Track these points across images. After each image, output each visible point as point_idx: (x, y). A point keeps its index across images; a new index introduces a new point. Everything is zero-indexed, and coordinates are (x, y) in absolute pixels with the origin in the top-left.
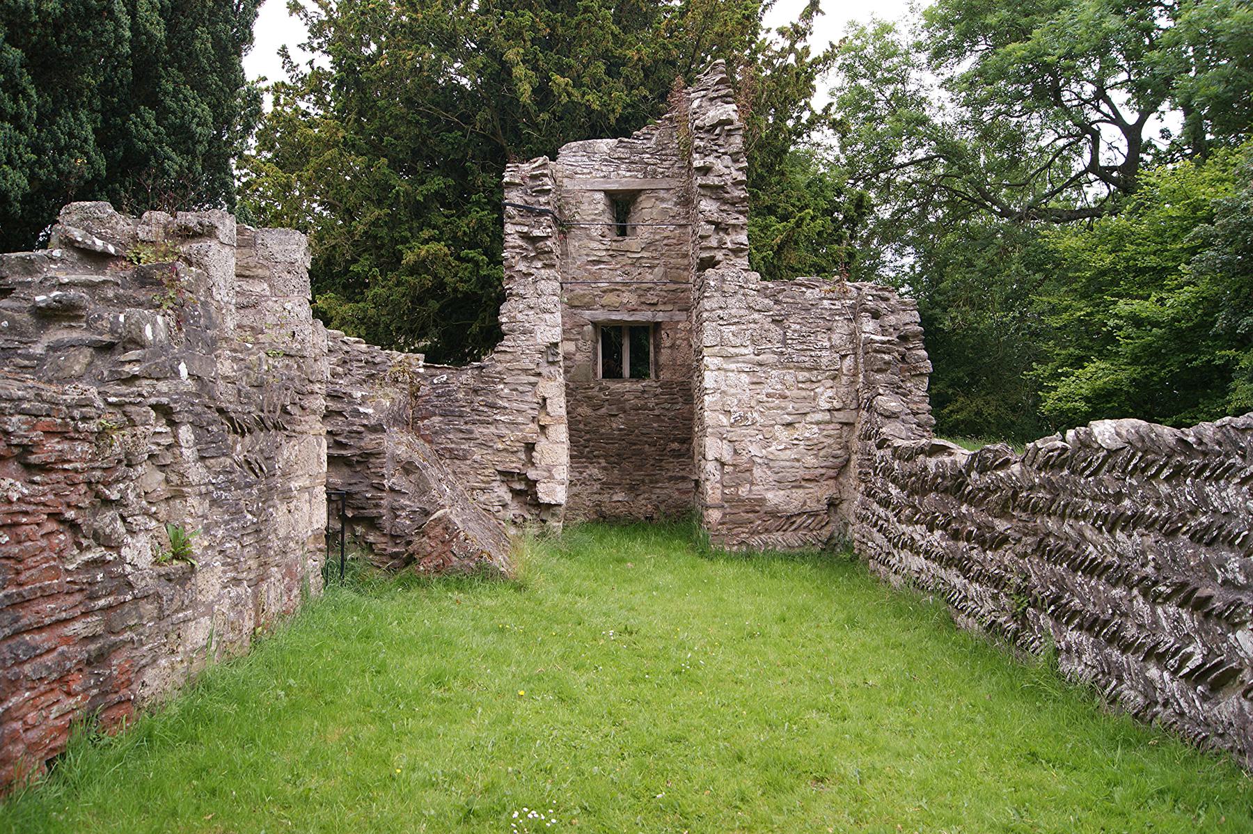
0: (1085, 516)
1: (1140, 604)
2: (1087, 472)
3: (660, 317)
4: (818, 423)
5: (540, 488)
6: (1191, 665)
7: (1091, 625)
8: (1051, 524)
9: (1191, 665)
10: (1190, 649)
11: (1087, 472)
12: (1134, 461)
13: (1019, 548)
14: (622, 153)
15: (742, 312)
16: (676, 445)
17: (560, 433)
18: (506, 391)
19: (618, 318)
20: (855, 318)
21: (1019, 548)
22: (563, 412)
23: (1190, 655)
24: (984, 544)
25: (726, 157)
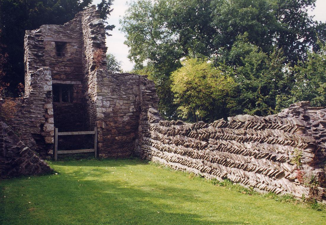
0: (234, 139)
1: (253, 159)
2: (236, 128)
3: (73, 83)
4: (130, 116)
5: (46, 138)
6: (271, 172)
7: (238, 167)
8: (224, 142)
9: (271, 172)
10: (270, 168)
11: (236, 128)
12: (250, 125)
13: (211, 149)
14: (61, 30)
15: (107, 82)
16: (78, 123)
17: (51, 120)
18: (34, 106)
19: (59, 83)
20: (138, 86)
21: (211, 149)
22: (52, 113)
23: (270, 170)
24: (197, 148)
25: (100, 35)
